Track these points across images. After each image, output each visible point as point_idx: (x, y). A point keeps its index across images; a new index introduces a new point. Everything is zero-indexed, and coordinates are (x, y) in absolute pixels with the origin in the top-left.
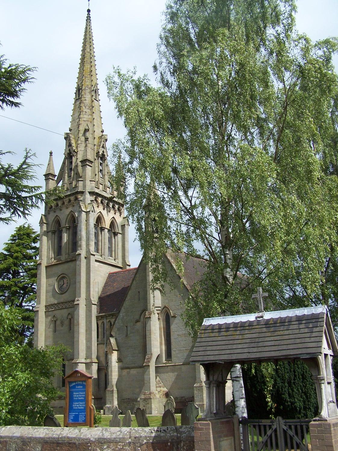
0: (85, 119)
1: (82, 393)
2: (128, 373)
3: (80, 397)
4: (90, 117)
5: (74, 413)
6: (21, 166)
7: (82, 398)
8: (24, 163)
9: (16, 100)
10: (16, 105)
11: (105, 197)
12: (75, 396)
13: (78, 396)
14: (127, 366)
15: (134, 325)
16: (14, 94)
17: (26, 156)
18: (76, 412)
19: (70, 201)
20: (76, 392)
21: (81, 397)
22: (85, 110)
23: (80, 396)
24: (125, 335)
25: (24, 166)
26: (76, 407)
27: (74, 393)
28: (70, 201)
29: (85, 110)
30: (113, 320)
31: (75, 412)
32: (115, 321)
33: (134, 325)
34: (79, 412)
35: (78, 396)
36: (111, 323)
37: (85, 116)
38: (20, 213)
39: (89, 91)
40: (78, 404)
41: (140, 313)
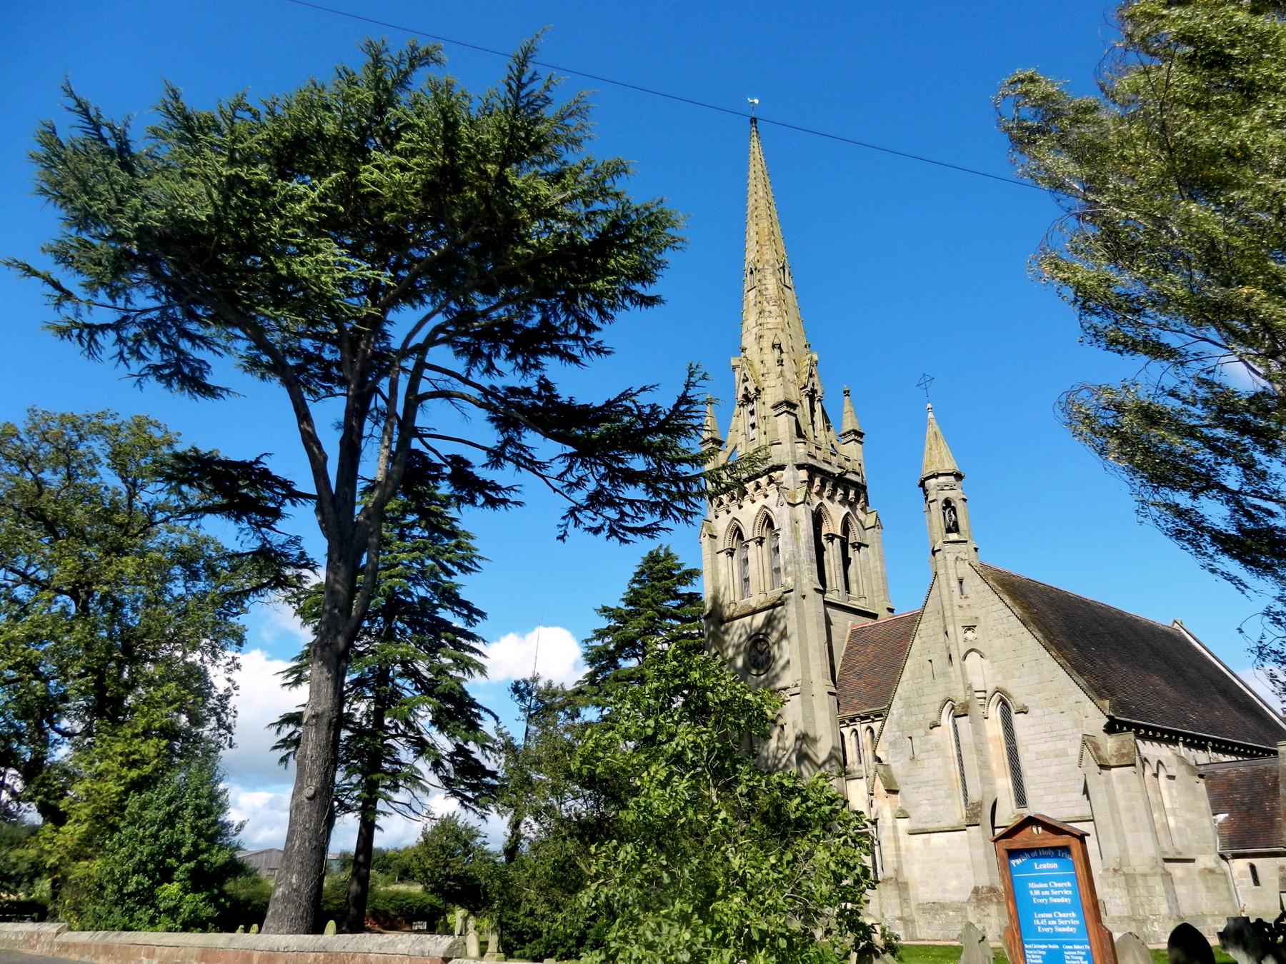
0: (770, 326)
1: (1060, 885)
2: (927, 843)
3: (1055, 897)
4: (779, 319)
5: (1044, 947)
6: (676, 407)
7: (1063, 900)
8: (684, 399)
9: (649, 291)
10: (649, 301)
11: (829, 473)
12: (1037, 893)
13: (1047, 893)
14: (921, 826)
15: (927, 734)
16: (643, 275)
17: (689, 382)
18: (1052, 943)
19: (758, 487)
20: (1038, 880)
21: (1059, 896)
22: (767, 309)
23: (1055, 893)
24: (907, 759)
25: (682, 408)
26: (1048, 926)
27: (1032, 885)
28: (758, 487)
29: (767, 309)
30: (876, 726)
31: (1046, 943)
32: (883, 726)
33: (927, 734)
34: (1060, 944)
35: (1047, 893)
36: (872, 732)
37: (769, 320)
38: (676, 513)
39: (771, 270)
40: (1054, 919)
41: (938, 706)
